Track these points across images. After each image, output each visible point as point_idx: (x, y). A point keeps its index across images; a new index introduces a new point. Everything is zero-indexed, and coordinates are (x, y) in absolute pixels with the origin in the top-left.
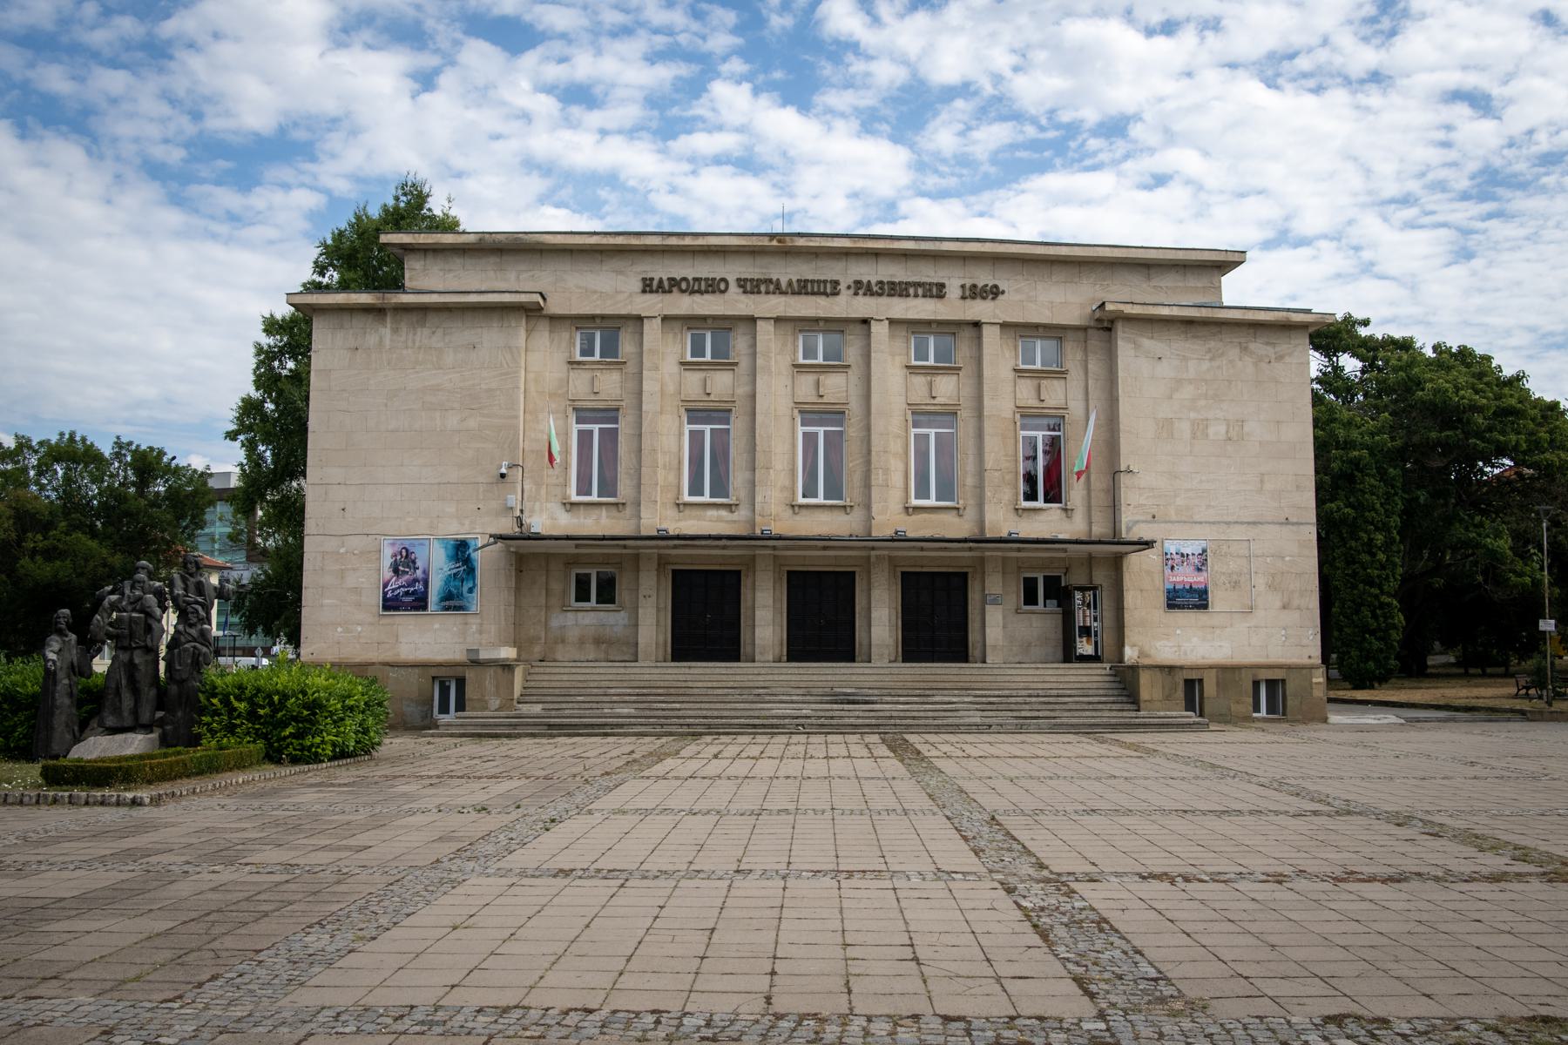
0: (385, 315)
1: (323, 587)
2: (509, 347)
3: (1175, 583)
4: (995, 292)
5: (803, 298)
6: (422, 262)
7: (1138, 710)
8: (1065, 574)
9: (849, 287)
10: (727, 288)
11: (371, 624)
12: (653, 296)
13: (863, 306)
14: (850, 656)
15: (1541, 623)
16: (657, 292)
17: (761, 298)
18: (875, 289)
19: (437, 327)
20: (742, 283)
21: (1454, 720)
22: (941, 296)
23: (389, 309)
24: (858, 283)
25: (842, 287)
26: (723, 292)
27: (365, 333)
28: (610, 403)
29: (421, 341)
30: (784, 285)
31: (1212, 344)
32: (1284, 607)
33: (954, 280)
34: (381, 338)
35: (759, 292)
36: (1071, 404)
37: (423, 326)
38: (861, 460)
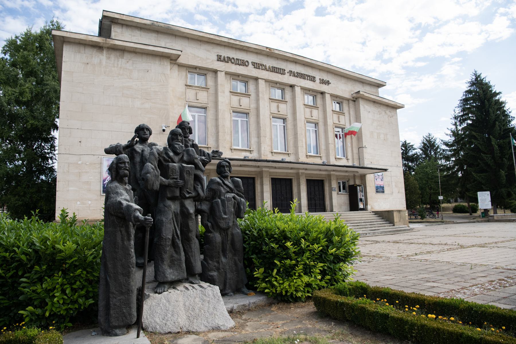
0: (103, 50)
1: (68, 181)
2: (164, 74)
3: (377, 184)
4: (328, 83)
5: (274, 73)
6: (121, 30)
7: (394, 225)
8: (348, 181)
9: (288, 73)
10: (248, 64)
11: (96, 200)
12: (222, 63)
13: (292, 80)
14: (324, 210)
15: (439, 197)
16: (222, 61)
17: (260, 71)
18: (296, 75)
19: (130, 60)
20: (254, 64)
21: (432, 225)
22: (314, 81)
23: (105, 48)
24: (291, 72)
25: (286, 72)
26: (247, 66)
27: (92, 57)
28: (203, 105)
29: (121, 65)
30: (267, 68)
31: (379, 110)
32: (399, 192)
33: (319, 76)
34: (101, 60)
35: (259, 69)
36: (347, 124)
37: (123, 58)
38: (292, 137)
